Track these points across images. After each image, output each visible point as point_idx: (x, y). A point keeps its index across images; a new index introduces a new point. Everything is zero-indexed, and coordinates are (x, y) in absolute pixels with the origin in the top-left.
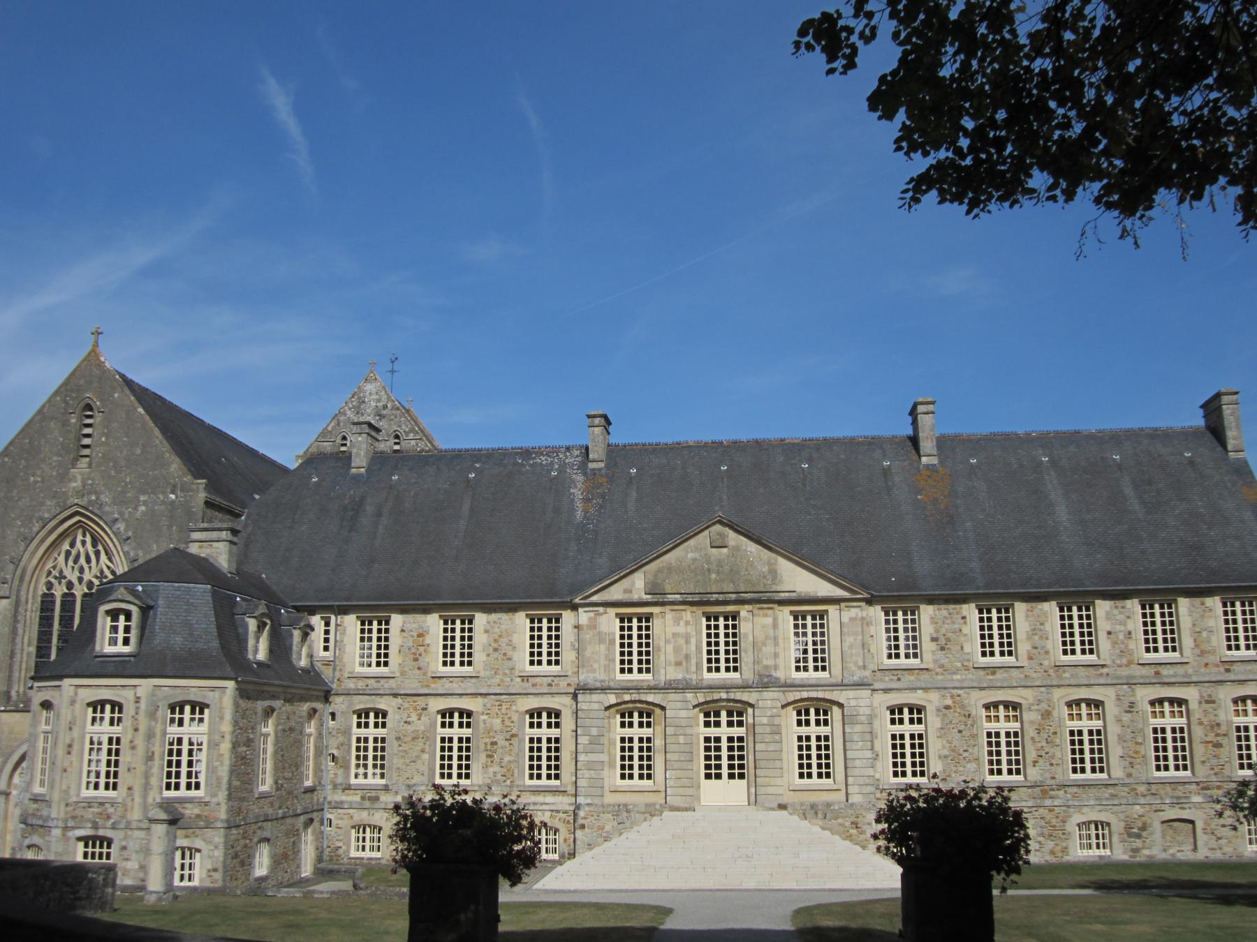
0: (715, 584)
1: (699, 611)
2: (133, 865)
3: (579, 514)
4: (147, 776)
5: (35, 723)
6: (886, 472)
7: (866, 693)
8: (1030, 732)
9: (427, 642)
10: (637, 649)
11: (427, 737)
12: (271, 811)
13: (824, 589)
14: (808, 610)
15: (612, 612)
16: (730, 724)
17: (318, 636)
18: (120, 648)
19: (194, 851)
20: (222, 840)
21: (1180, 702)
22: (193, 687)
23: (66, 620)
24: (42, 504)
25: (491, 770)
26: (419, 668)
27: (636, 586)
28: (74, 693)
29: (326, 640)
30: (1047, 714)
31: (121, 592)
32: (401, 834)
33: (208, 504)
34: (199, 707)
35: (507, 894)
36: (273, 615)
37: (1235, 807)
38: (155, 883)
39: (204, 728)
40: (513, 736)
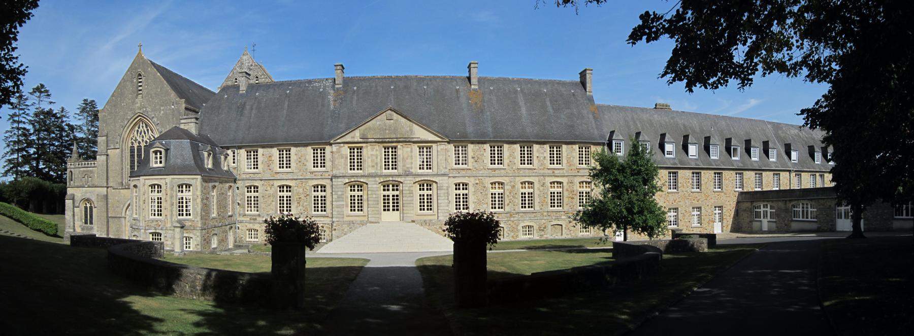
0: (387, 135)
1: (381, 145)
2: (169, 243)
3: (332, 107)
4: (172, 211)
5: (132, 193)
6: (457, 91)
7: (446, 178)
8: (507, 193)
10: (357, 161)
11: (274, 196)
12: (217, 224)
13: (432, 137)
14: (425, 146)
15: (347, 146)
16: (393, 190)
17: (230, 158)
18: (159, 165)
19: (190, 238)
21: (561, 183)
22: (185, 179)
23: (139, 156)
27: (356, 135)
28: (144, 182)
30: (513, 187)
31: (157, 144)
32: (267, 231)
33: (186, 109)
34: (188, 186)
35: (308, 254)
36: (213, 150)
37: (575, 219)
38: (177, 249)
39: (191, 193)
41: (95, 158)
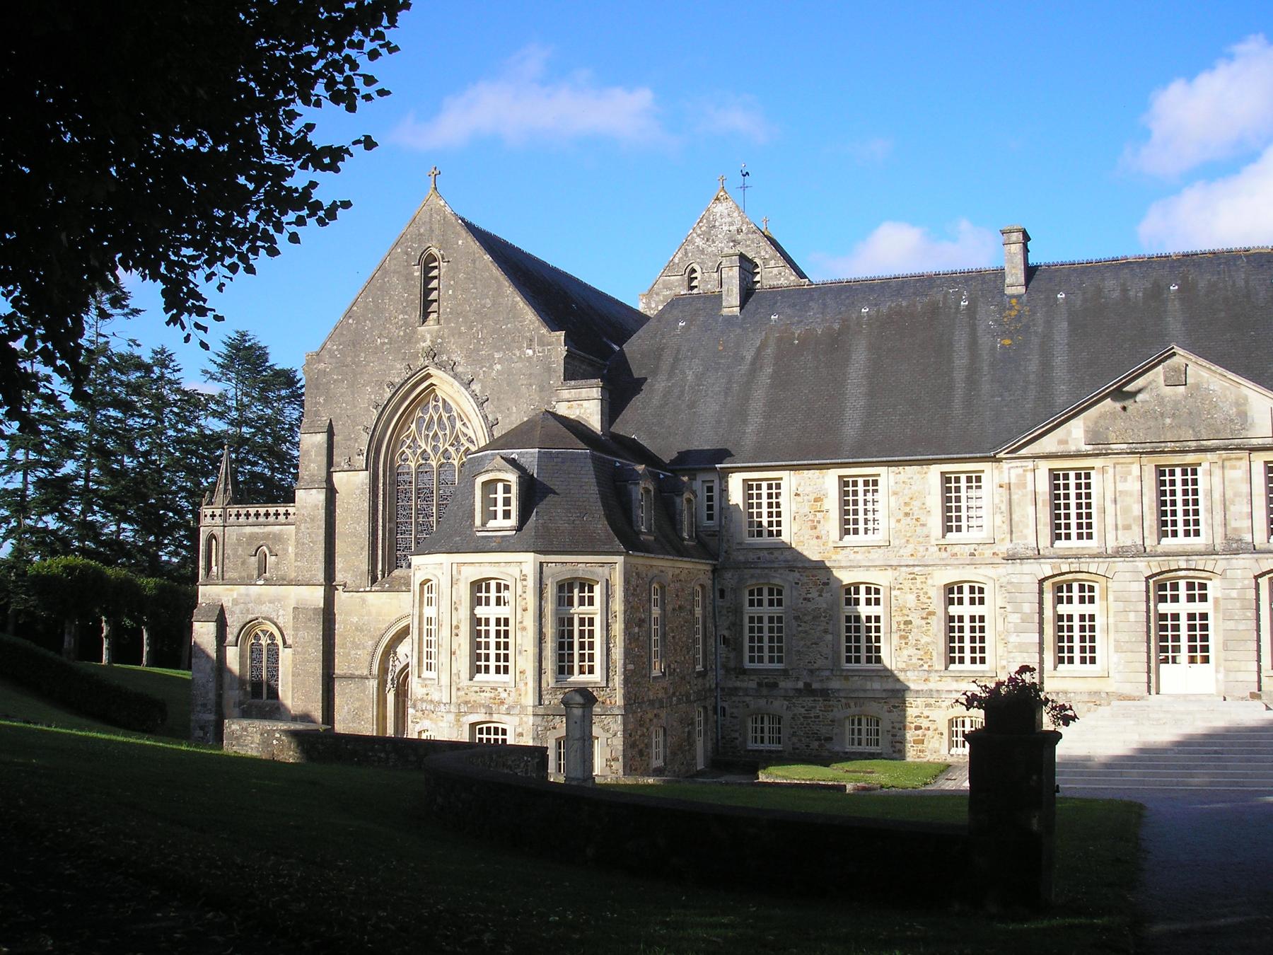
9: (825, 508)
20: (621, 728)
24: (392, 367)
25: (905, 653)
26: (818, 537)
29: (710, 508)
40: (930, 614)
41: (289, 498)
